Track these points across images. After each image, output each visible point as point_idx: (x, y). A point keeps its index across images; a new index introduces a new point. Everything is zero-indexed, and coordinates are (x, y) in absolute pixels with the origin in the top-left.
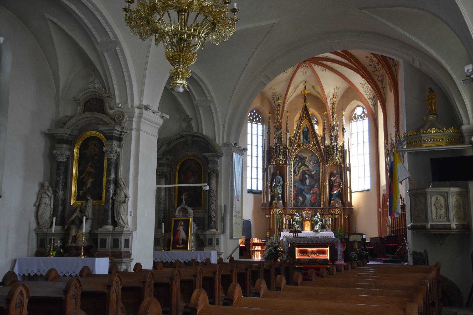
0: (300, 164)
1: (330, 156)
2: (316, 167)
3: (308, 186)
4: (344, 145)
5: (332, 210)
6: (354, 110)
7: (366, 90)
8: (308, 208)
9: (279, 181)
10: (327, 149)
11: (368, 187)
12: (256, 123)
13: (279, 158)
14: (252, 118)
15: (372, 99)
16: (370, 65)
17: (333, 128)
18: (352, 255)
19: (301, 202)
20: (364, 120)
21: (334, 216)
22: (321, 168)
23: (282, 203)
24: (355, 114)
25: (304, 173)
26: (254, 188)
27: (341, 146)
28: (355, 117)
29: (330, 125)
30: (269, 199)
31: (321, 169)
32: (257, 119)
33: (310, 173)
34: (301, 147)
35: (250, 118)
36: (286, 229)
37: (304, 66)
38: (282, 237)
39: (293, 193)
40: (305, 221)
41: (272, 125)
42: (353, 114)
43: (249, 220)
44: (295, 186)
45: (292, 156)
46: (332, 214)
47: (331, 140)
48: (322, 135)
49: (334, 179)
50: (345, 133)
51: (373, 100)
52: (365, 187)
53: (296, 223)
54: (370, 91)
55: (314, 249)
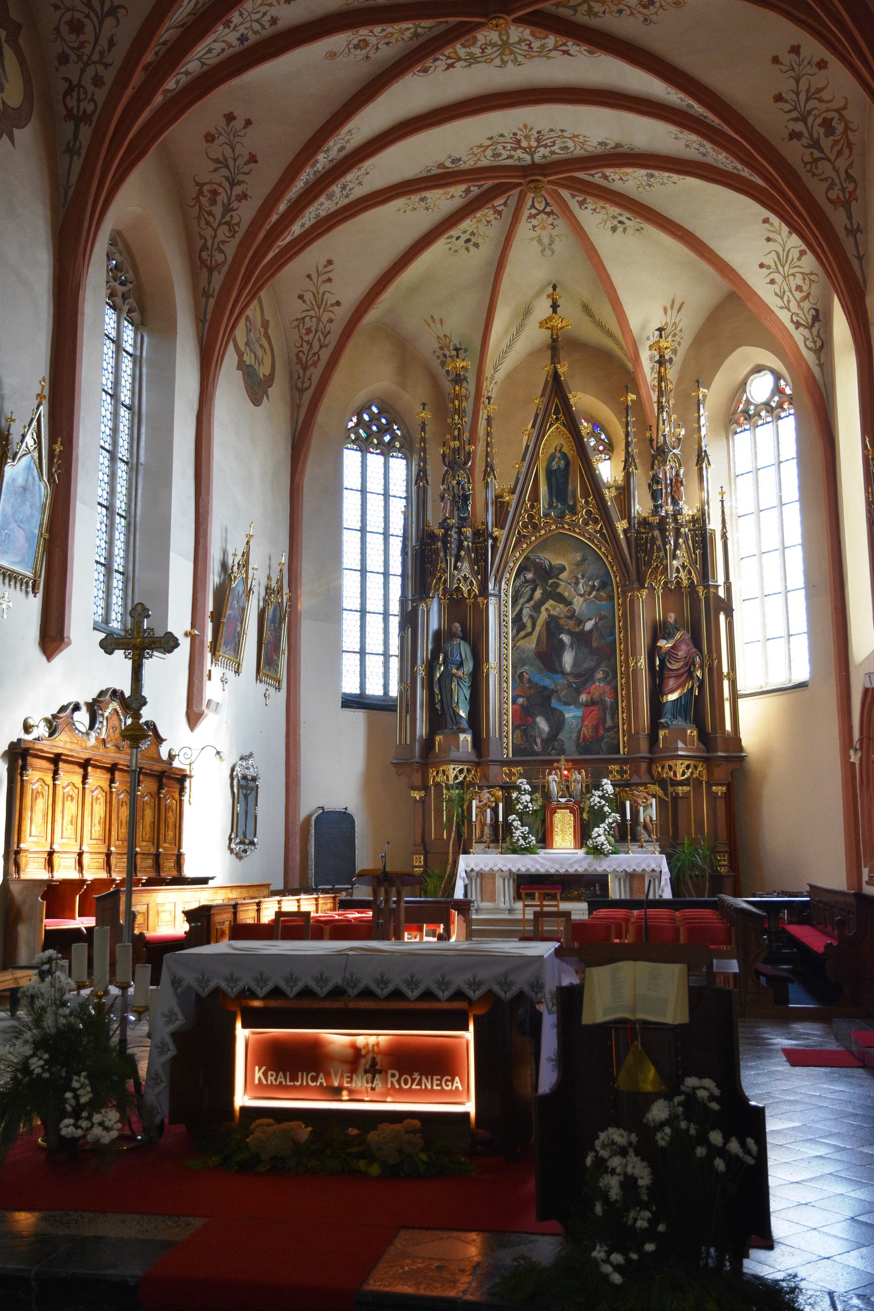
0: (538, 594)
1: (651, 558)
2: (598, 602)
3: (568, 674)
4: (703, 514)
5: (663, 768)
6: (742, 386)
7: (784, 292)
8: (567, 761)
9: (458, 658)
10: (638, 532)
11: (802, 672)
12: (382, 454)
13: (456, 572)
14: (364, 435)
15: (810, 327)
16: (794, 135)
17: (658, 454)
18: (601, 1164)
19: (544, 736)
20: (780, 418)
21: (670, 789)
22: (619, 605)
23: (470, 744)
24: (748, 400)
25: (553, 627)
26: (374, 689)
27: (694, 520)
28: (746, 411)
29: (651, 440)
30: (421, 729)
31: (619, 610)
32: (387, 438)
33: (579, 625)
34: (542, 529)
35: (357, 434)
36: (485, 842)
37: (540, 212)
38: (464, 875)
39: (514, 702)
40: (554, 812)
41: (435, 452)
42: (741, 402)
43: (346, 809)
44: (519, 678)
45: (506, 563)
46: (662, 783)
47: (655, 495)
48: (620, 482)
49: (670, 645)
50: (709, 470)
51: (815, 330)
52: (791, 674)
53: (521, 820)
54: (798, 295)
55: (372, 1040)
